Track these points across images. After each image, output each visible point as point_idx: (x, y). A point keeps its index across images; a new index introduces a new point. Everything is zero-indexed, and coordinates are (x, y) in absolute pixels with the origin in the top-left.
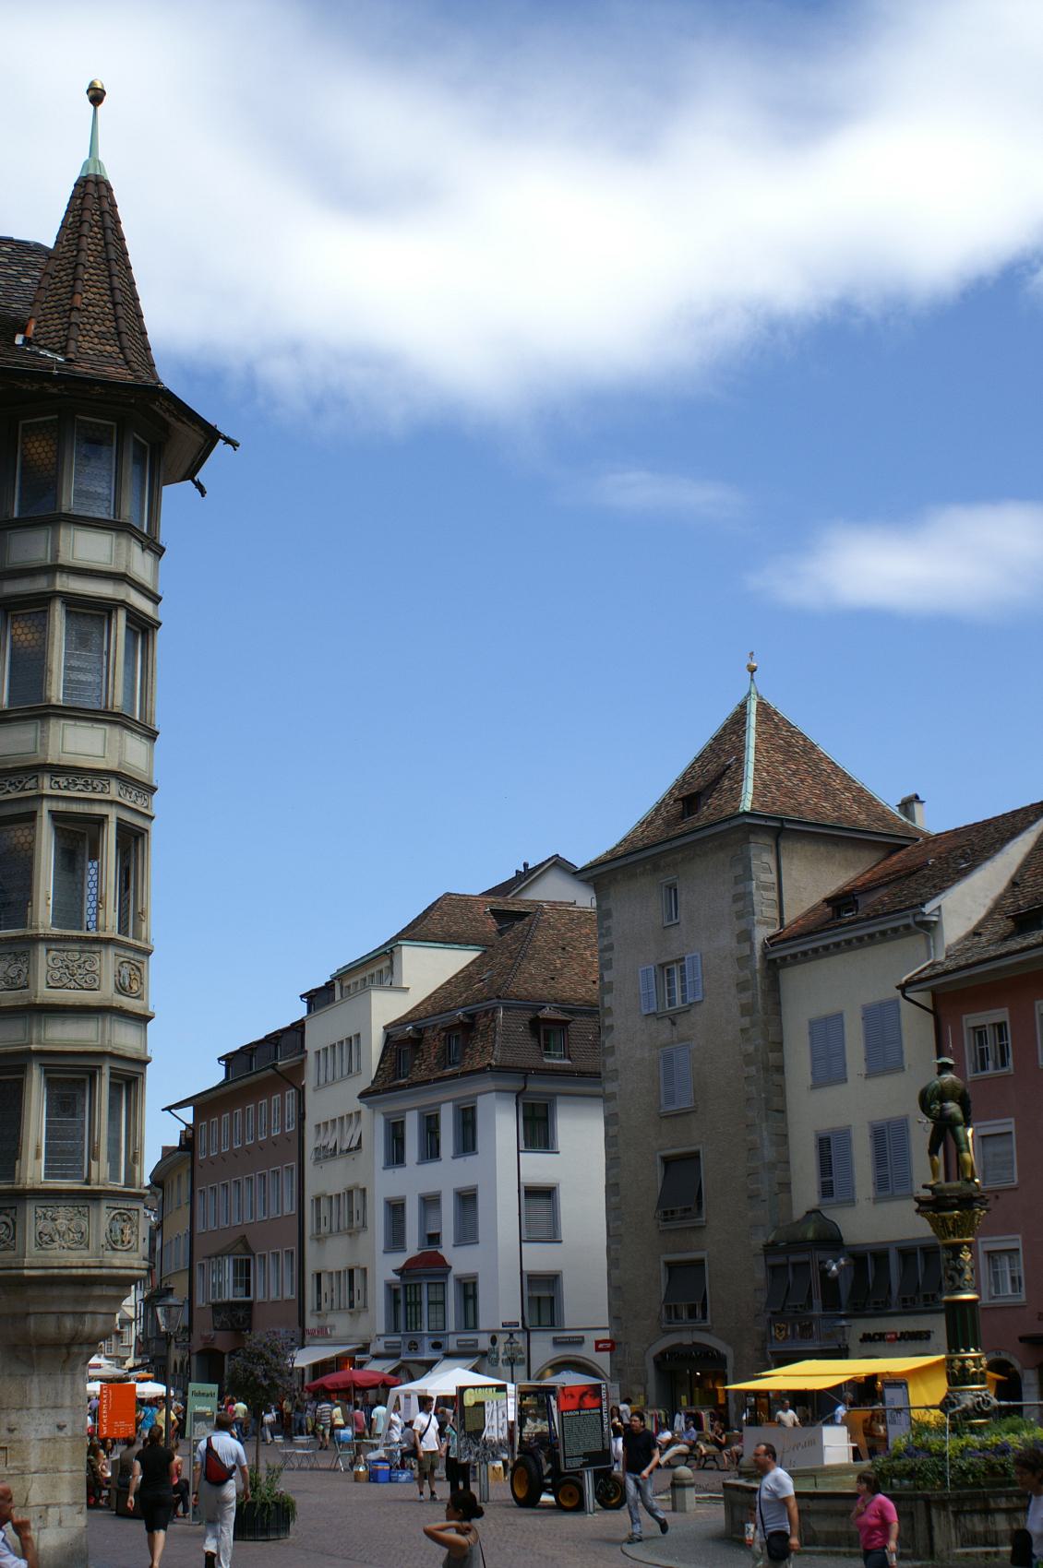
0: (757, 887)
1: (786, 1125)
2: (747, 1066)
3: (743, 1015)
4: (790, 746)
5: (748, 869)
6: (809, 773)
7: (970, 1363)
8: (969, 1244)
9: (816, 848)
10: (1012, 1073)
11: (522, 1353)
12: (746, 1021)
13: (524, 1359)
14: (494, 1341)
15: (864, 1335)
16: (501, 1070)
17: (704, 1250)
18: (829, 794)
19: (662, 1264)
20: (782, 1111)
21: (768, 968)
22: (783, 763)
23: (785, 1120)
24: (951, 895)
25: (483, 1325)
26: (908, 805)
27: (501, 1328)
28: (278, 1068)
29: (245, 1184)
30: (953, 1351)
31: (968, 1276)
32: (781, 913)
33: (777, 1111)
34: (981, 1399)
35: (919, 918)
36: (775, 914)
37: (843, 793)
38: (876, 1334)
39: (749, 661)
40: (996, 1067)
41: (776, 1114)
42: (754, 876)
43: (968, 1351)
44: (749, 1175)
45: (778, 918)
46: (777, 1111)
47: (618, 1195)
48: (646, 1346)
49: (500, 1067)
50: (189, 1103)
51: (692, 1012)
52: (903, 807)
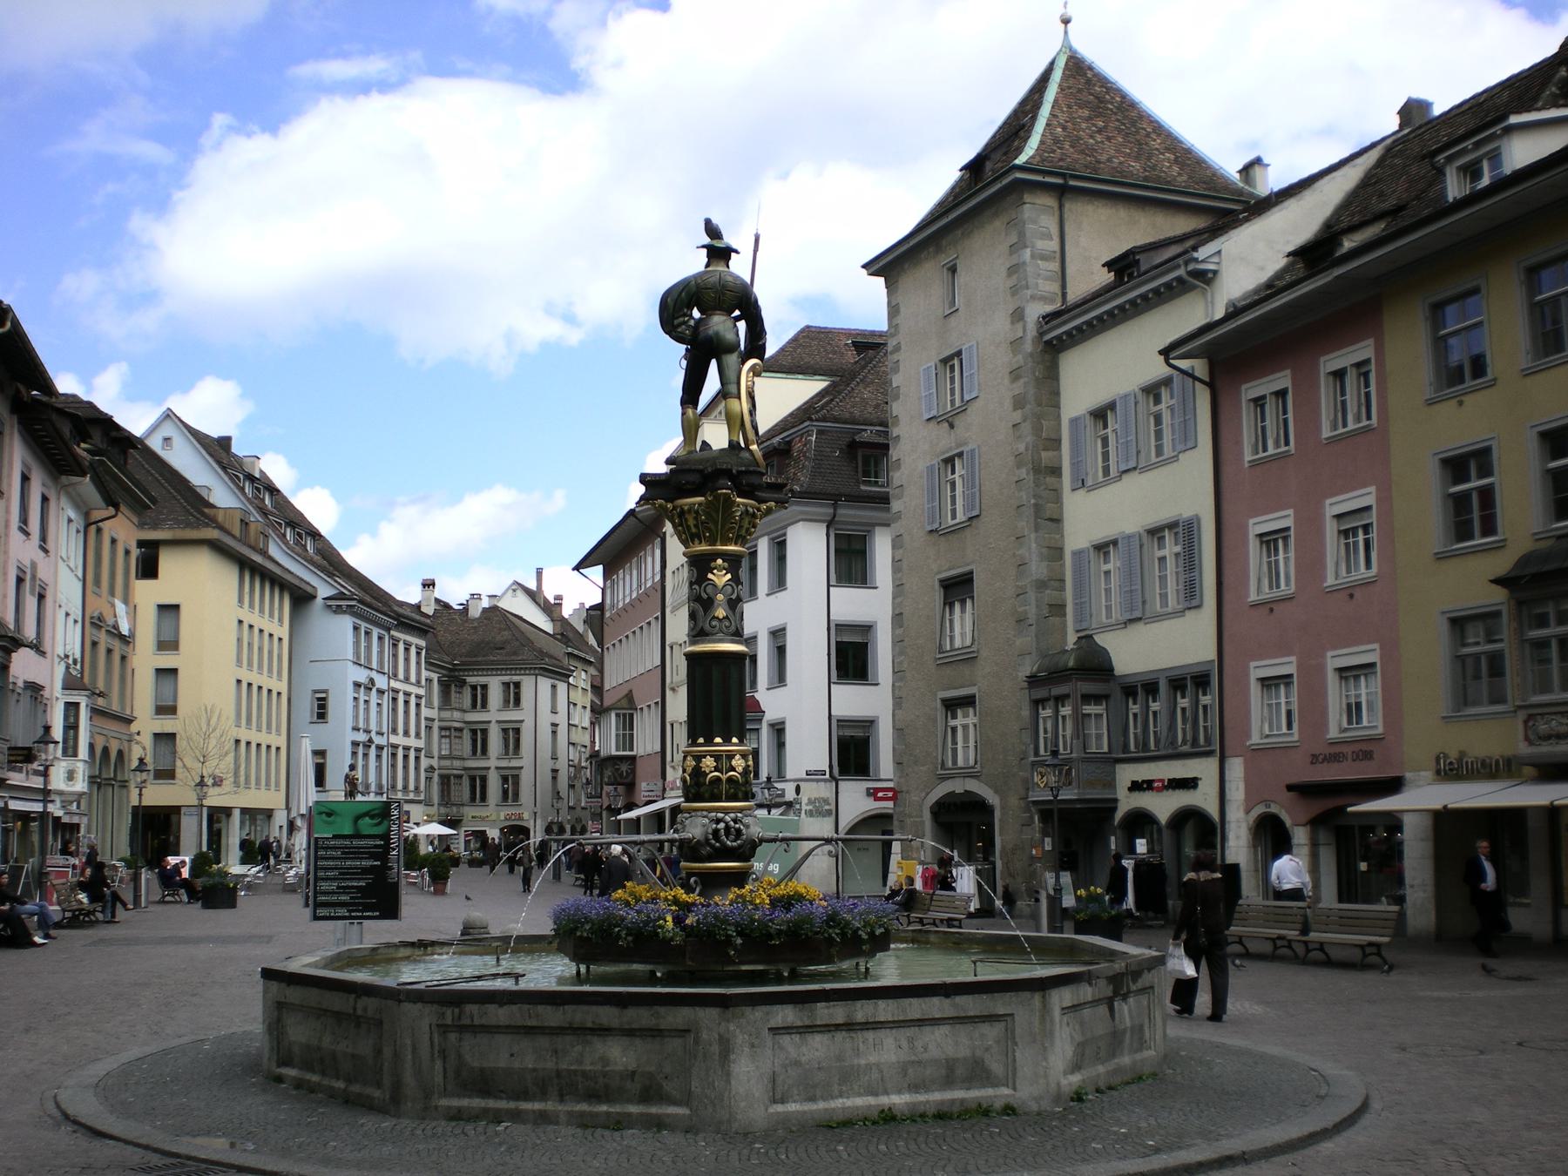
0: (1033, 256)
1: (1063, 536)
2: (1018, 468)
3: (1015, 409)
4: (1102, 102)
5: (1022, 235)
6: (1120, 131)
7: (709, 762)
8: (725, 556)
9: (1114, 210)
10: (1293, 452)
11: (829, 804)
12: (1017, 416)
13: (831, 810)
14: (798, 790)
15: (1133, 782)
16: (808, 495)
17: (975, 685)
18: (1142, 152)
19: (939, 701)
20: (1057, 521)
21: (1044, 351)
22: (1089, 119)
23: (1060, 532)
24: (1235, 239)
25: (789, 775)
26: (1251, 172)
27: (804, 776)
28: (639, 516)
29: (631, 636)
30: (701, 740)
31: (721, 613)
32: (1064, 286)
33: (1051, 520)
34: (722, 825)
35: (1191, 267)
36: (1054, 287)
37: (1163, 154)
38: (1143, 781)
39: (1062, 11)
40: (1277, 445)
41: (1049, 523)
42: (1028, 243)
43: (727, 741)
44: (1018, 595)
45: (1060, 294)
46: (1051, 520)
47: (901, 627)
48: (924, 794)
49: (805, 493)
50: (588, 562)
51: (969, 409)
52: (1244, 173)
